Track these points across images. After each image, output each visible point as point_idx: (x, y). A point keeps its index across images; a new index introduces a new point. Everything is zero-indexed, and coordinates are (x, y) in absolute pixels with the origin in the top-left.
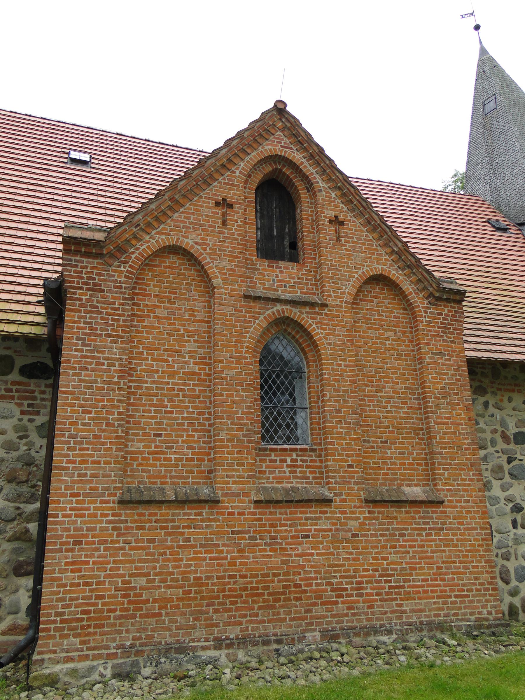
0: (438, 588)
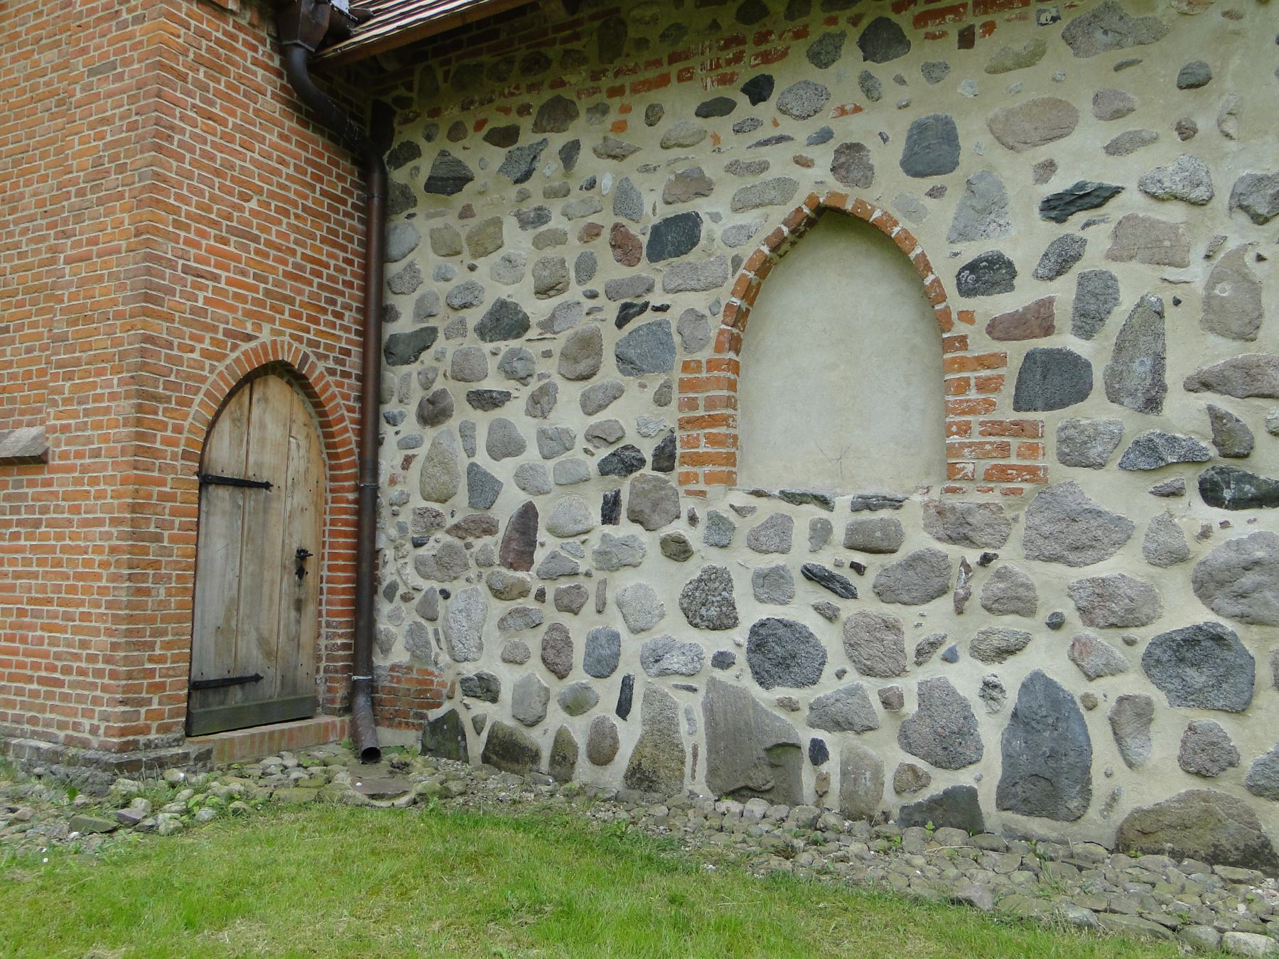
0: (14, 658)
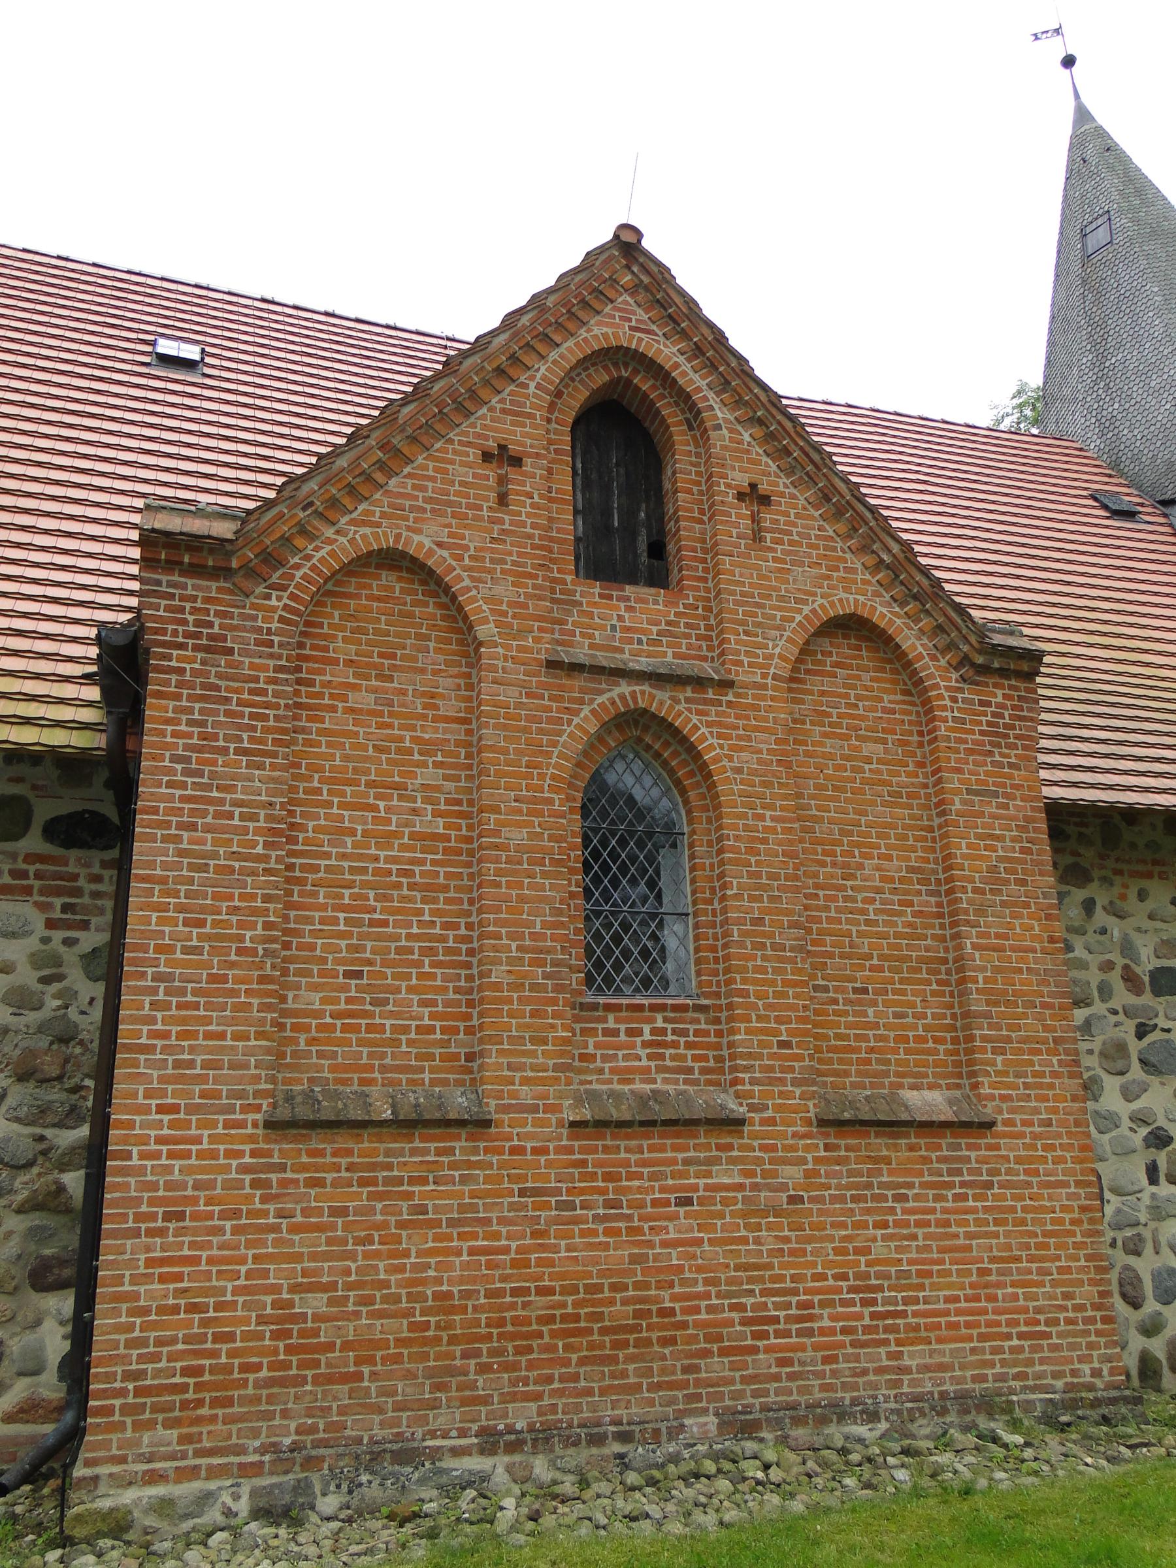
0: (982, 1318)
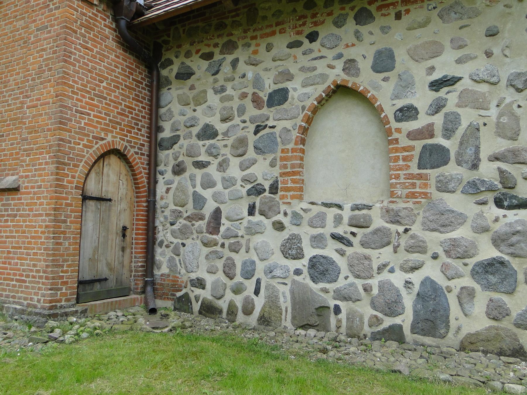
0: (6, 271)
